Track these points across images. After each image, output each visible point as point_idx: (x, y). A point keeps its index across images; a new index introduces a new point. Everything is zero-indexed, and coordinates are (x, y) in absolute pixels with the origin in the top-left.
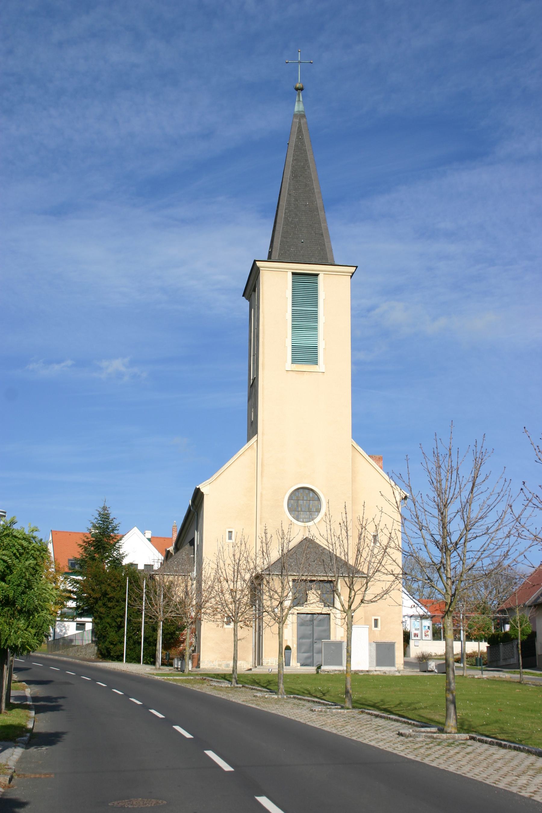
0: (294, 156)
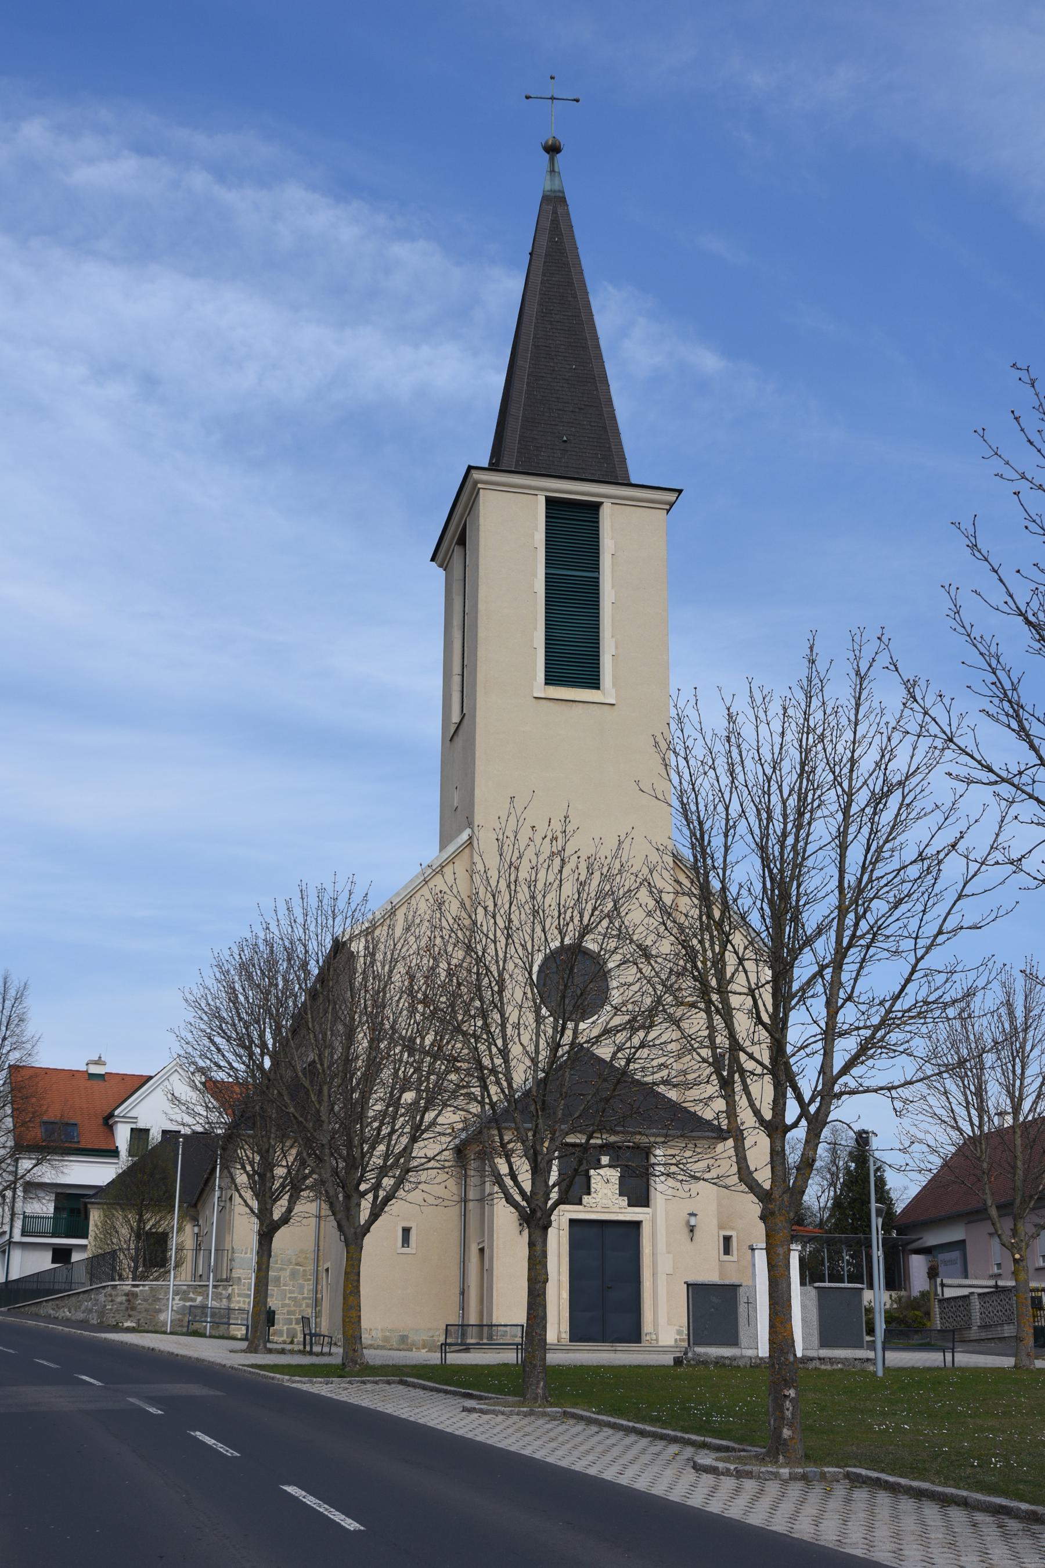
0: (544, 275)
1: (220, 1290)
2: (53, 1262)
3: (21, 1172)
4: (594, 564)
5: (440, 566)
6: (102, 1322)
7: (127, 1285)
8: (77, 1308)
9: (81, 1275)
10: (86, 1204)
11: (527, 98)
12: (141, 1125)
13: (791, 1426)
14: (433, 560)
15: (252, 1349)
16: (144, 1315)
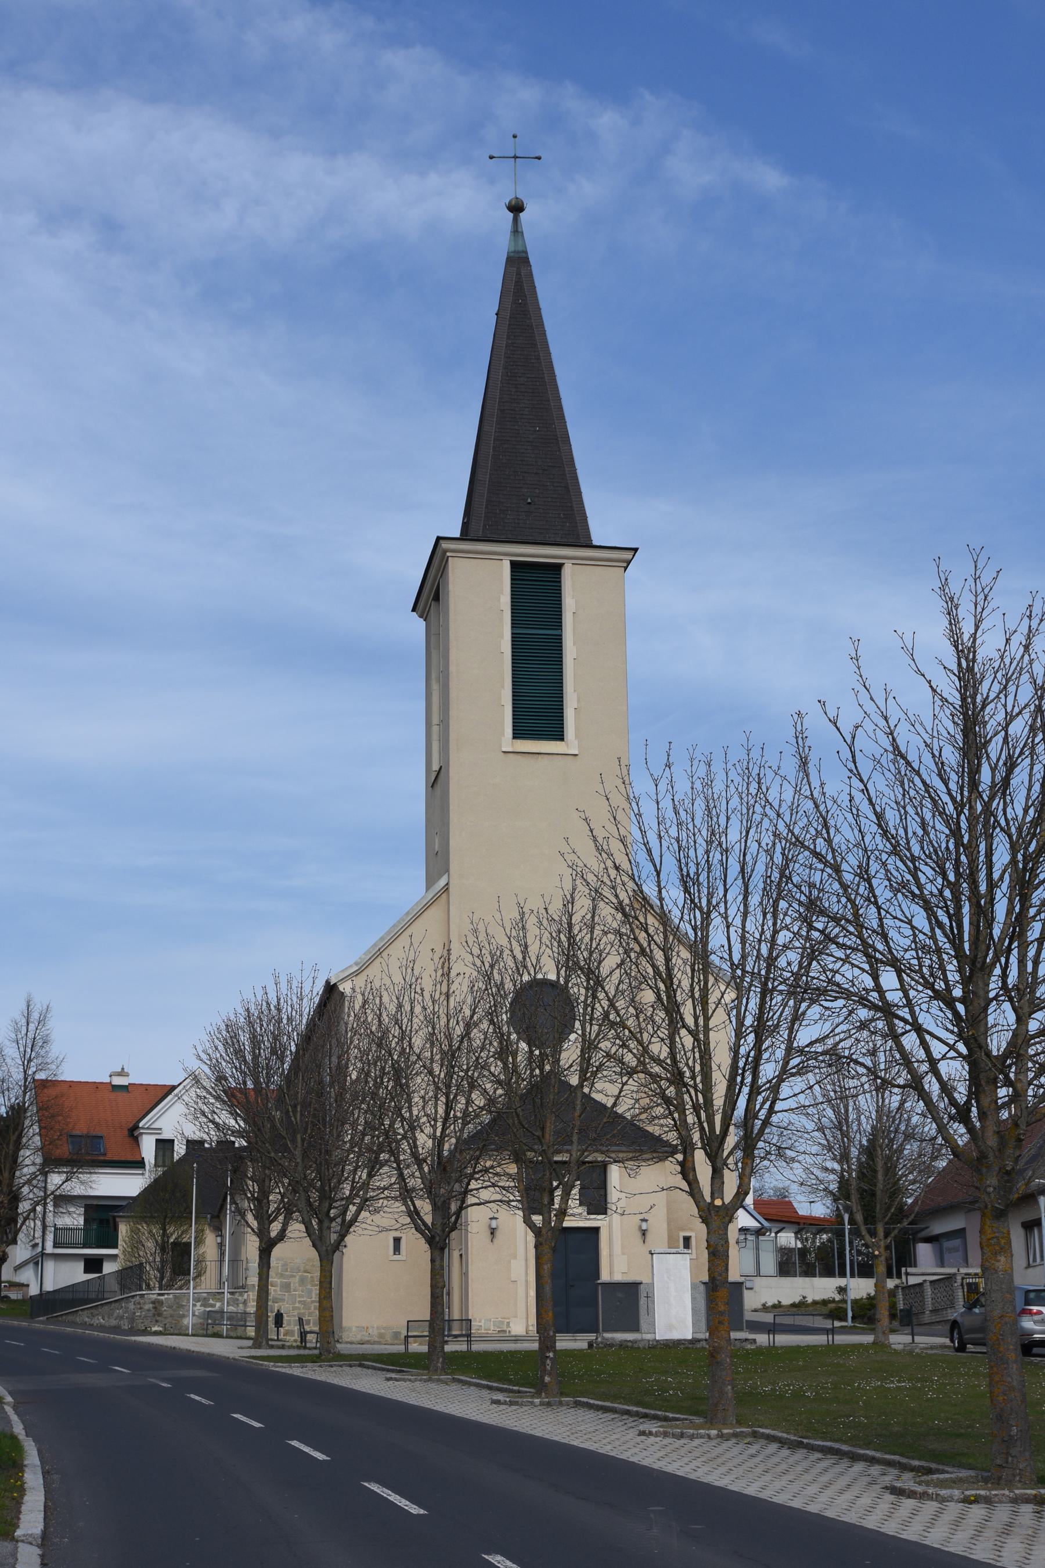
0: (508, 338)
1: (237, 1296)
2: (85, 1272)
3: (51, 1188)
4: (557, 622)
5: (421, 616)
6: (132, 1327)
7: (153, 1295)
8: (110, 1315)
9: (113, 1285)
10: (114, 1218)
11: (491, 157)
12: (166, 1135)
13: (550, 1375)
14: (414, 610)
15: (257, 1345)
16: (169, 1320)
